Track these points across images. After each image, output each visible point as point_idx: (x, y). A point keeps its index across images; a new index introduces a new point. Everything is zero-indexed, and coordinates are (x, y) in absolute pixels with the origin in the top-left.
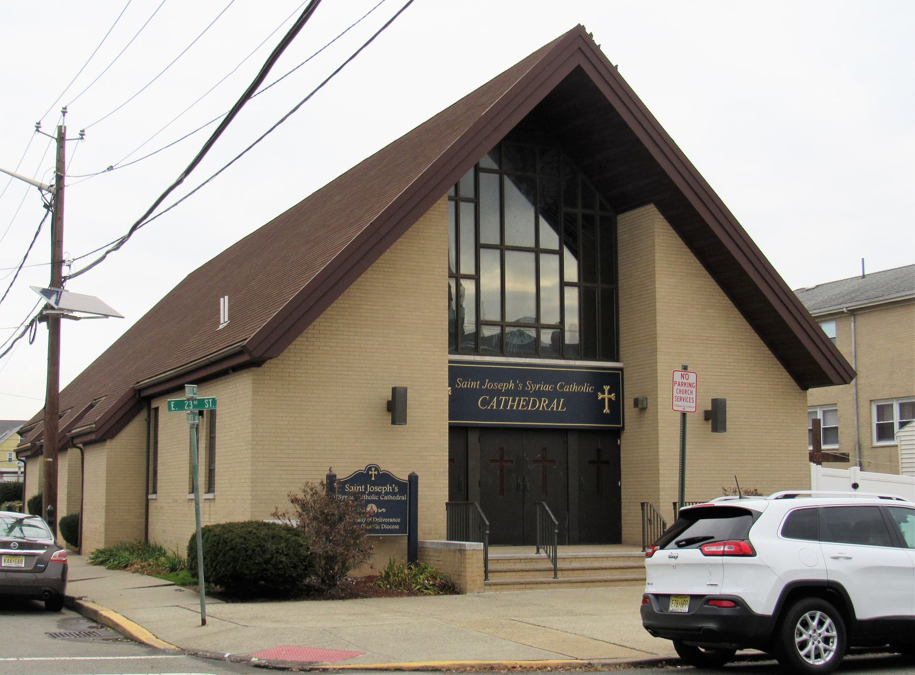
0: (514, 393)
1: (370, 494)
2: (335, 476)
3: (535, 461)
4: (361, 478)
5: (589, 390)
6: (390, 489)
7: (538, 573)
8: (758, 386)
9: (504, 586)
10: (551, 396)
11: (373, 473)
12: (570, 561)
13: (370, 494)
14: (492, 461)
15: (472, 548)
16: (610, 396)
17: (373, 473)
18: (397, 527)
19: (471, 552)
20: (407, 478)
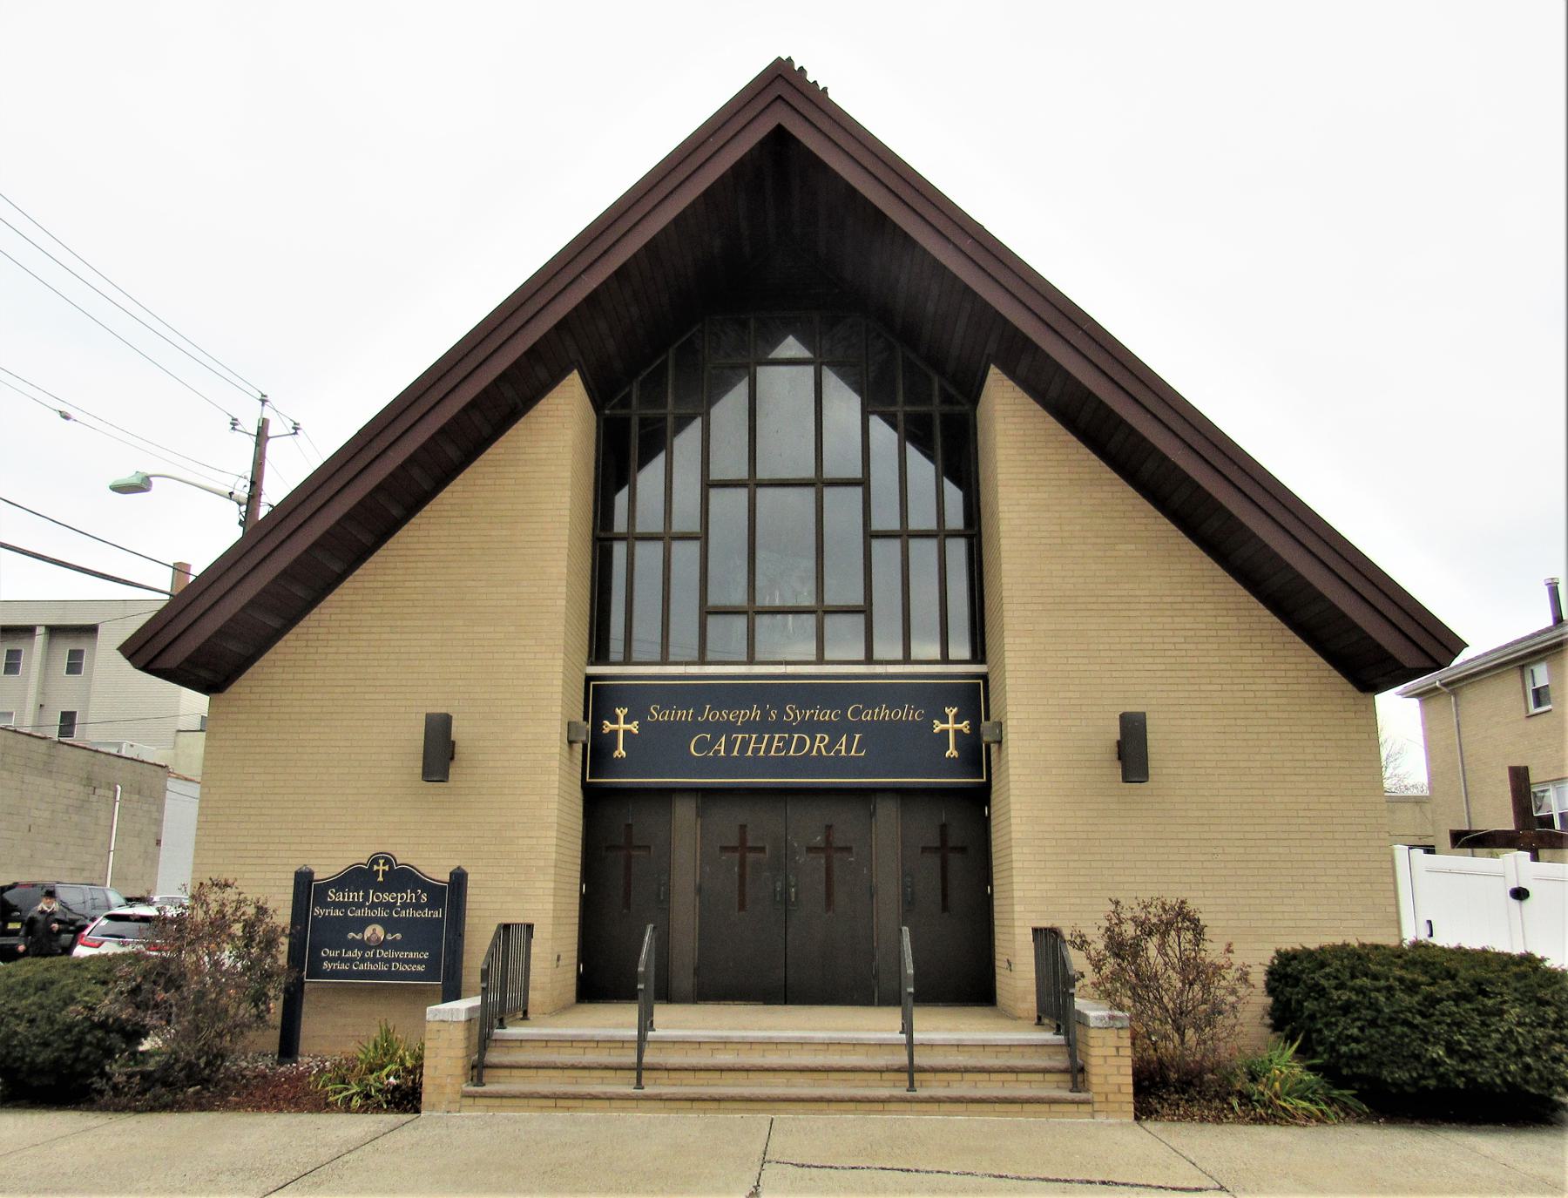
0: (761, 727)
1: (373, 906)
2: (311, 873)
3: (810, 849)
4: (357, 878)
5: (913, 716)
6: (411, 897)
7: (611, 1074)
8: (1247, 687)
9: (504, 1100)
10: (834, 730)
11: (381, 867)
12: (764, 1051)
13: (373, 906)
14: (724, 849)
15: (437, 1018)
16: (951, 719)
17: (381, 868)
18: (421, 968)
19: (435, 1027)
20: (447, 878)
